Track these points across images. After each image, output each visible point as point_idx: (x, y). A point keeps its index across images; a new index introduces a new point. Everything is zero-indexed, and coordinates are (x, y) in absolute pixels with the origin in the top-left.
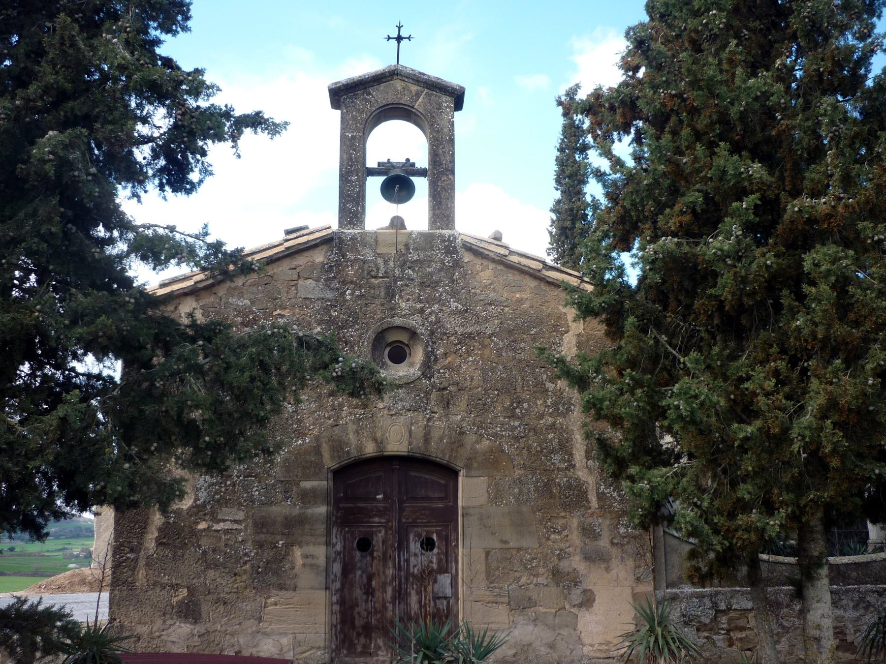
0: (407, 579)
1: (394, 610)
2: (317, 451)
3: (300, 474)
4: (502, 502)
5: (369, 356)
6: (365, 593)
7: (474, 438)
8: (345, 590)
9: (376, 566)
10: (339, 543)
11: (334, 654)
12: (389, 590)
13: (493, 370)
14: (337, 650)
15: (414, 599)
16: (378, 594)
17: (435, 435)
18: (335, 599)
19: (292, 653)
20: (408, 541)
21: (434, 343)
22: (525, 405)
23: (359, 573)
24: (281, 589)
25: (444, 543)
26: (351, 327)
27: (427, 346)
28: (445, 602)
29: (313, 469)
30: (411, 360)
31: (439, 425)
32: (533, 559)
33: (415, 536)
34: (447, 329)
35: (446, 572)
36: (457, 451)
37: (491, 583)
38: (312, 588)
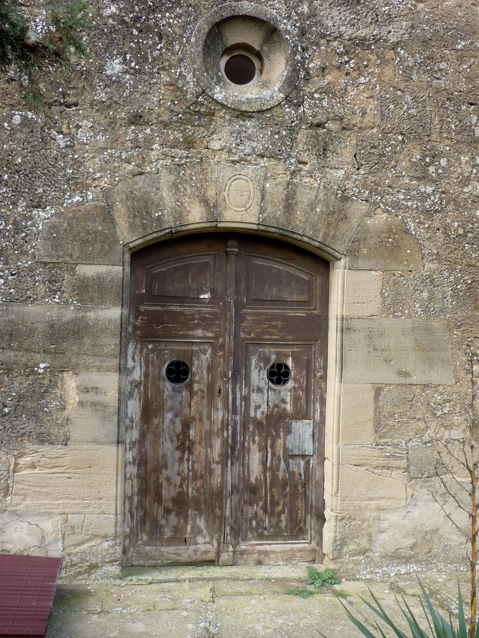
0: (245, 427)
1: (223, 475)
2: (107, 214)
3: (76, 253)
4: (402, 312)
5: (199, 61)
6: (177, 448)
7: (364, 207)
8: (147, 443)
9: (197, 406)
10: (138, 369)
11: (127, 541)
12: (217, 444)
13: (396, 101)
14: (132, 536)
15: (255, 459)
16: (199, 450)
17: (304, 198)
18: (130, 456)
19: (60, 544)
20: (248, 367)
21: (304, 49)
22: (443, 162)
23: (169, 416)
24: (42, 442)
25: (304, 373)
26: (168, 10)
27: (295, 53)
28: (302, 463)
29: (98, 246)
30: (264, 76)
31: (310, 188)
32: (446, 401)
33: (260, 360)
34: (326, 28)
35: (306, 416)
36: (336, 228)
37: (381, 437)
38: (95, 441)
